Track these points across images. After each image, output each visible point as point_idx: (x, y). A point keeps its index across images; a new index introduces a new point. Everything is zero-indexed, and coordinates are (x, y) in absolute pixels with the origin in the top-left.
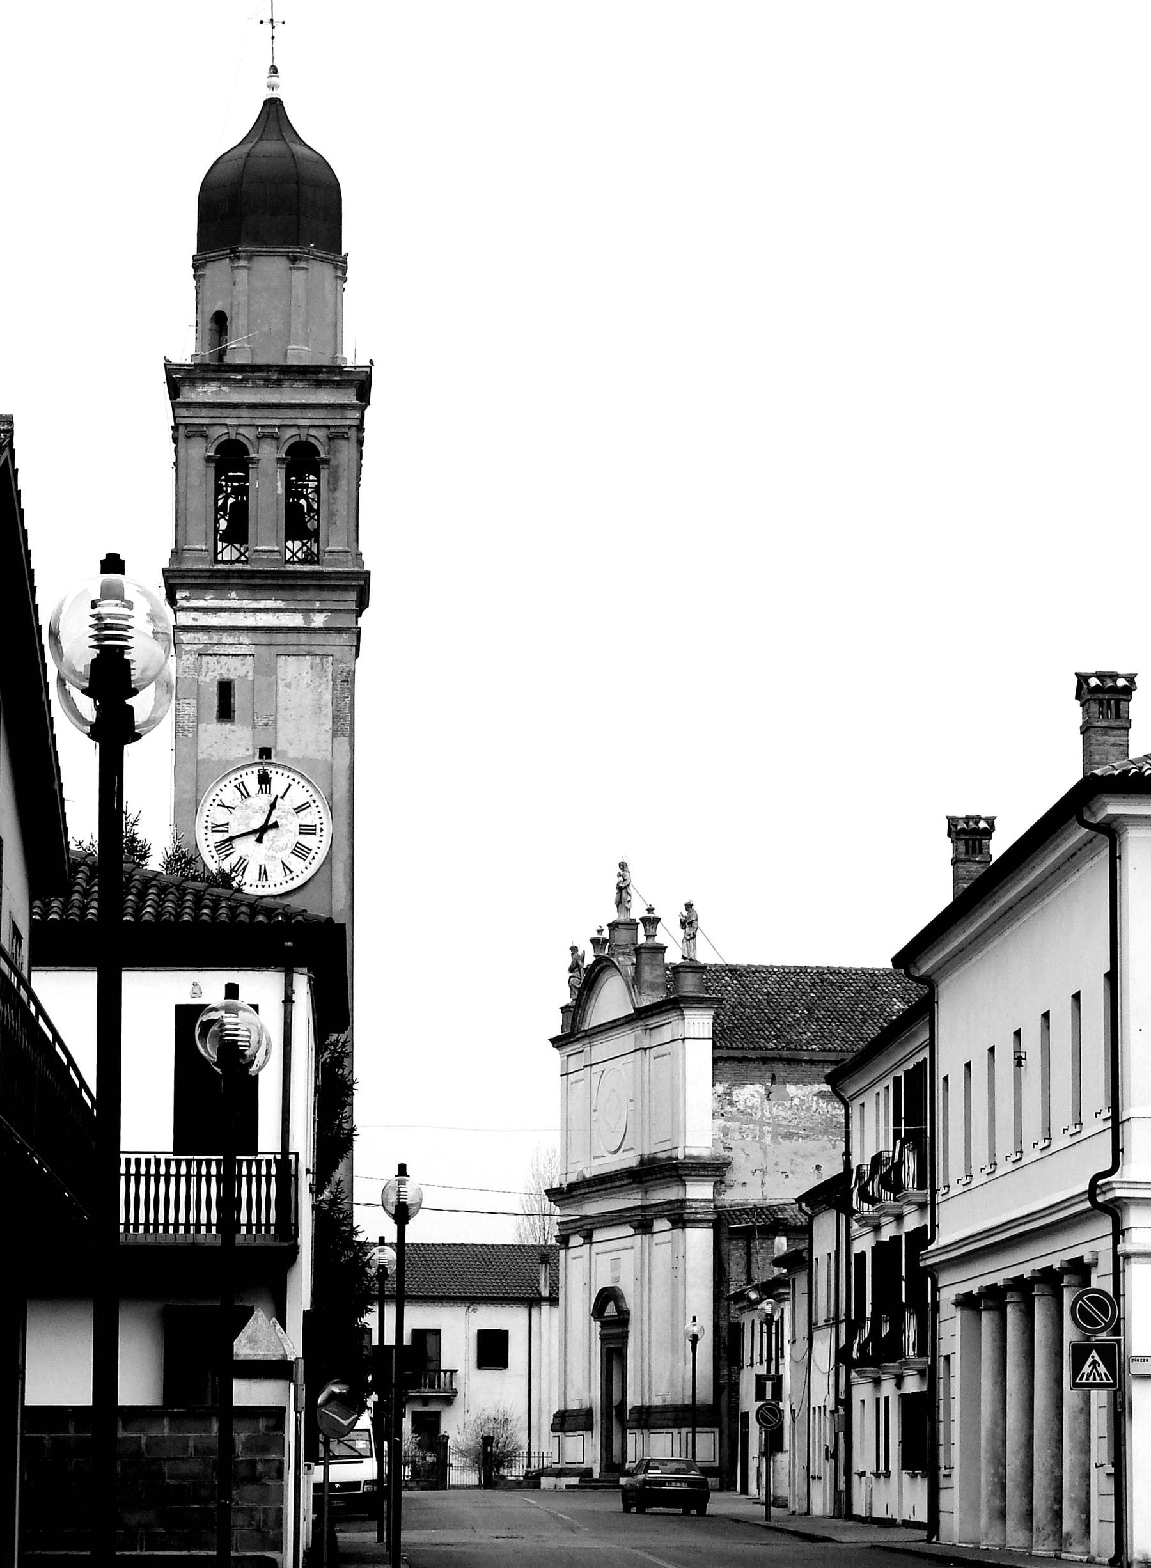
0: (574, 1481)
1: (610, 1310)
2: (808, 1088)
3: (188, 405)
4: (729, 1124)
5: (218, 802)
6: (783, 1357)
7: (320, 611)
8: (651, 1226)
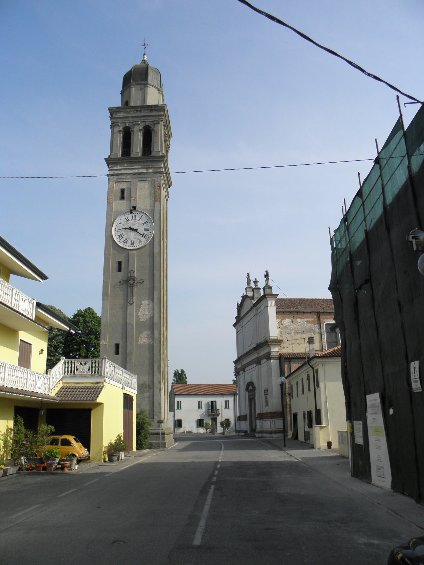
0: (243, 434)
1: (251, 387)
2: (303, 320)
3: (115, 118)
4: (282, 330)
5: (119, 223)
6: (318, 386)
7: (151, 168)
8: (260, 363)
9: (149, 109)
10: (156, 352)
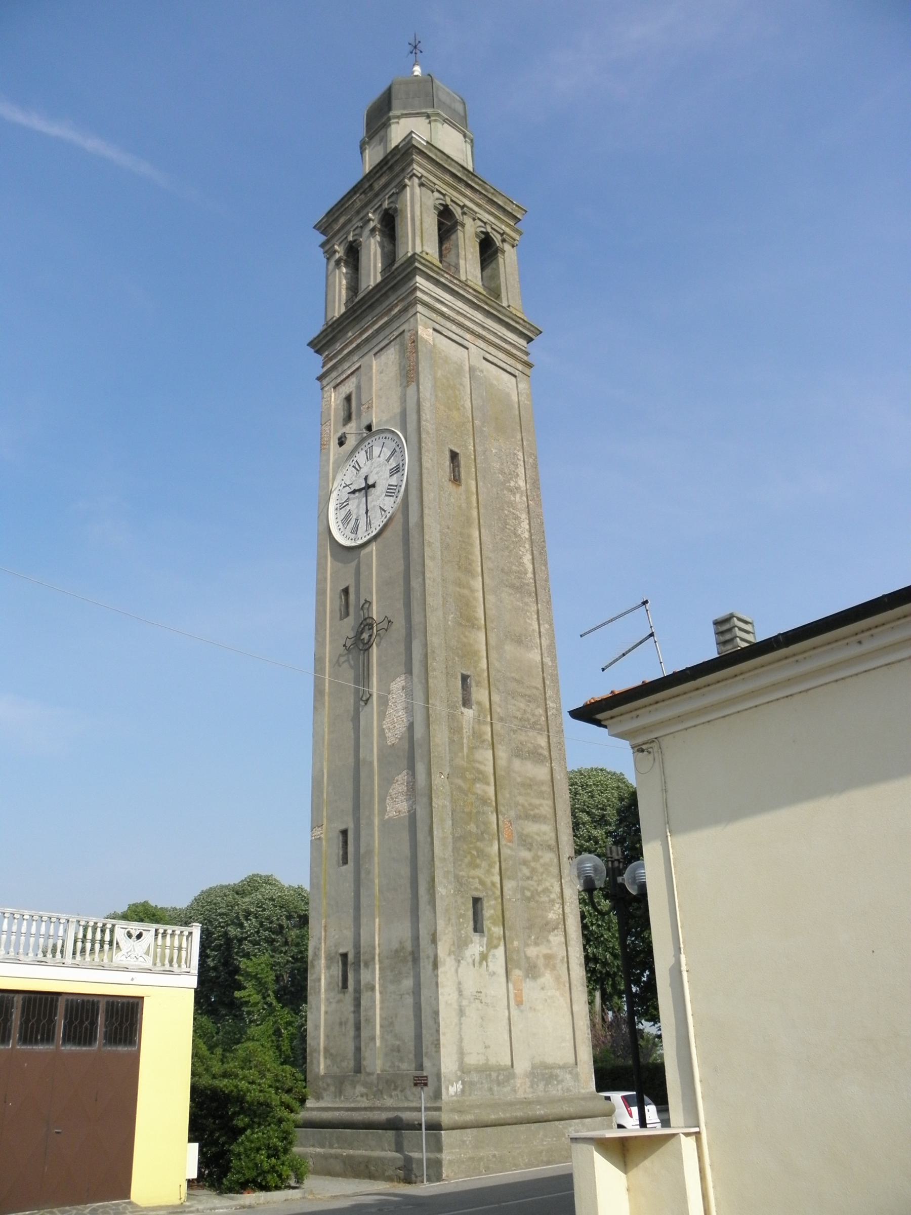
9: (385, 168)
10: (421, 836)
